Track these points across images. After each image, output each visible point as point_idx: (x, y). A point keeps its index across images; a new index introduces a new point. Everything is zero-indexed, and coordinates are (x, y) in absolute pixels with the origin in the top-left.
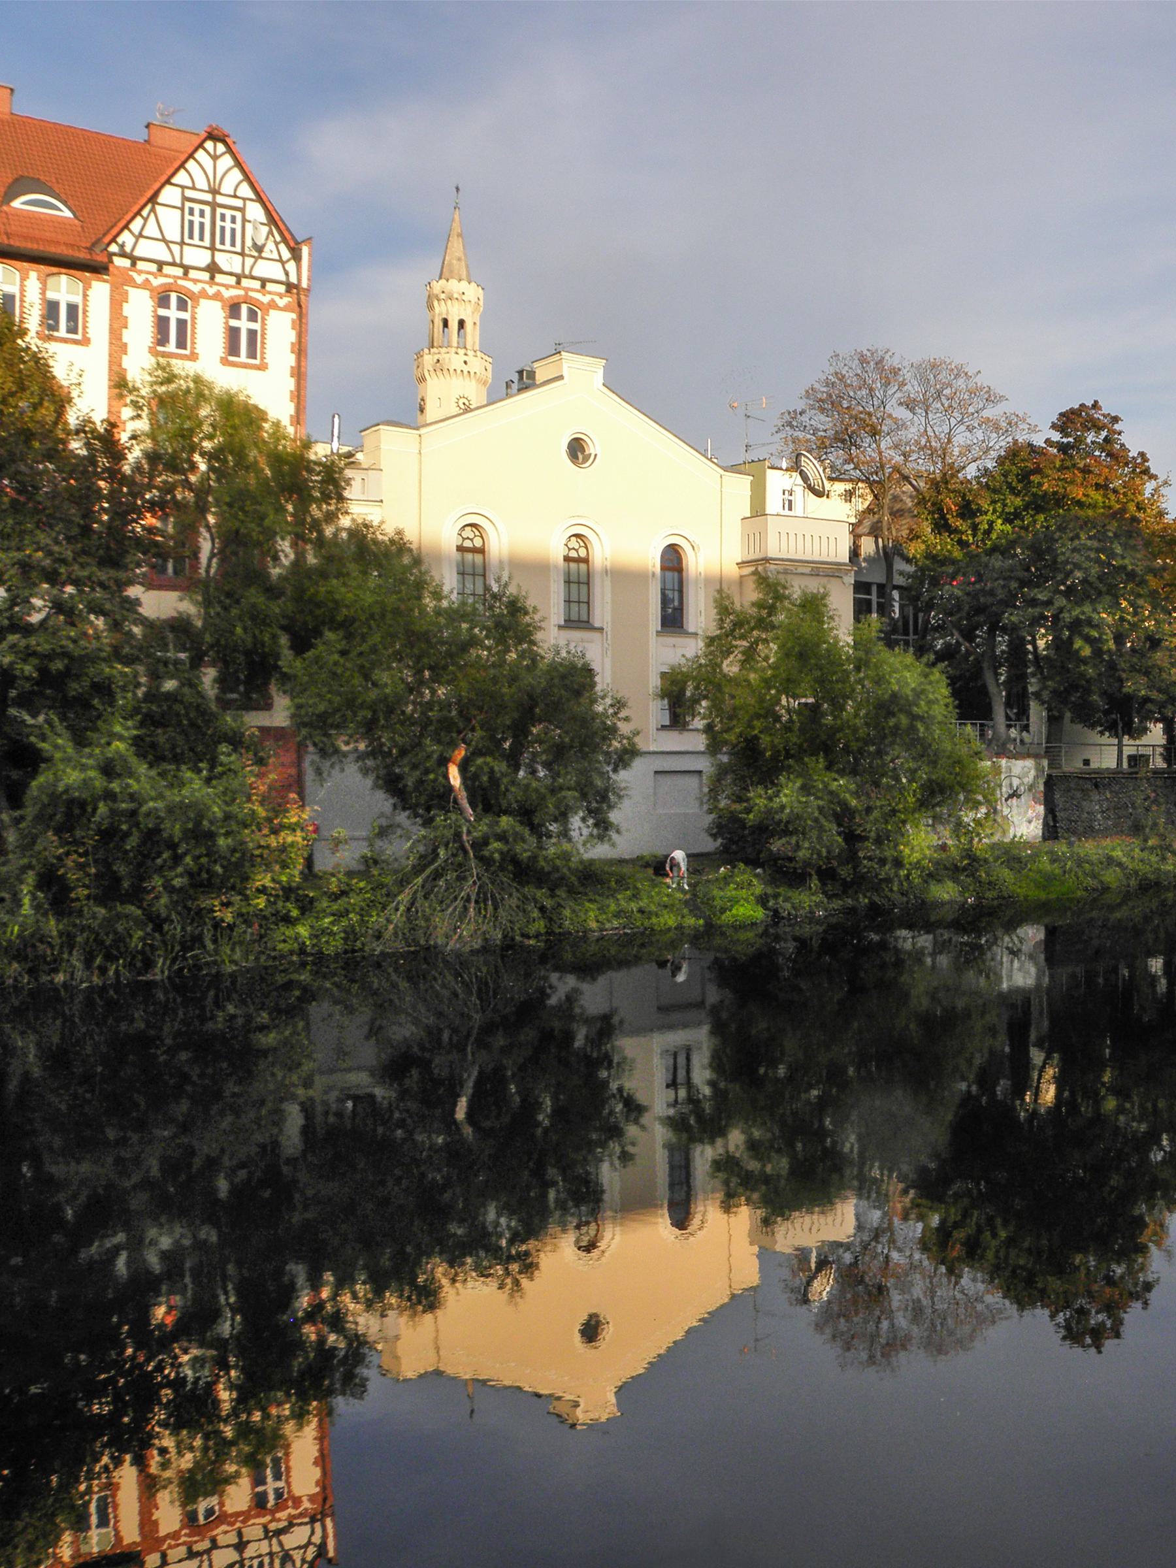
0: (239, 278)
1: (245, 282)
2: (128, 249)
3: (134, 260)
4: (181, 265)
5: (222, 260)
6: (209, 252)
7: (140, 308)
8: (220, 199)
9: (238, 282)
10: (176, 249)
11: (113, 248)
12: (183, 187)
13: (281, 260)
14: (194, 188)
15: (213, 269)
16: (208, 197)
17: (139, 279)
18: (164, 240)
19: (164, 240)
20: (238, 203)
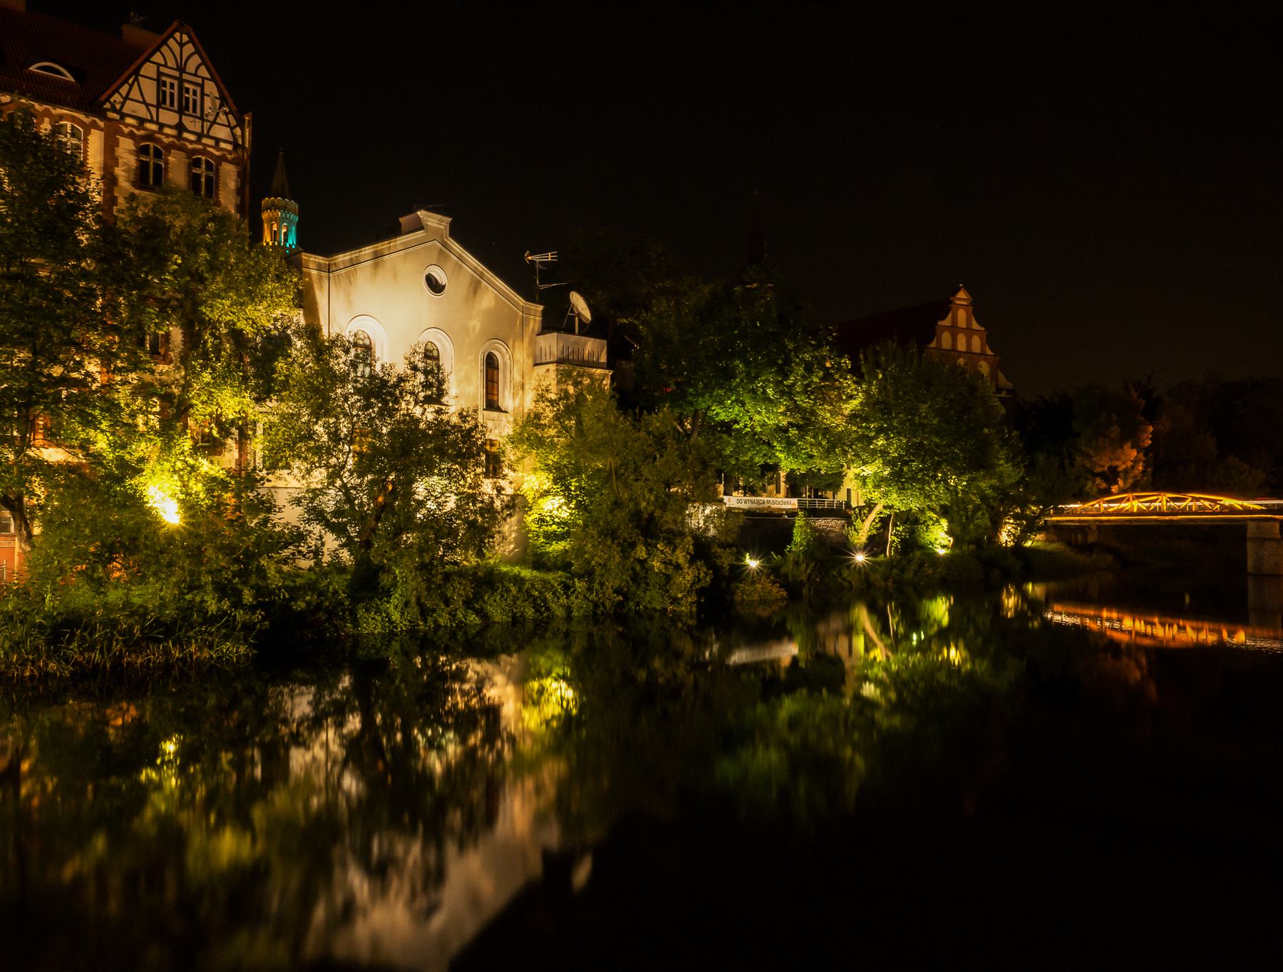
0: (200, 136)
1: (205, 141)
2: (118, 107)
3: (123, 116)
4: (157, 123)
5: (187, 121)
6: (177, 116)
7: (126, 147)
8: (185, 76)
9: (199, 141)
10: (153, 110)
11: (107, 106)
12: (159, 65)
13: (229, 126)
14: (166, 66)
15: (180, 128)
16: (176, 74)
17: (126, 130)
18: (144, 102)
19: (144, 102)
20: (200, 81)
